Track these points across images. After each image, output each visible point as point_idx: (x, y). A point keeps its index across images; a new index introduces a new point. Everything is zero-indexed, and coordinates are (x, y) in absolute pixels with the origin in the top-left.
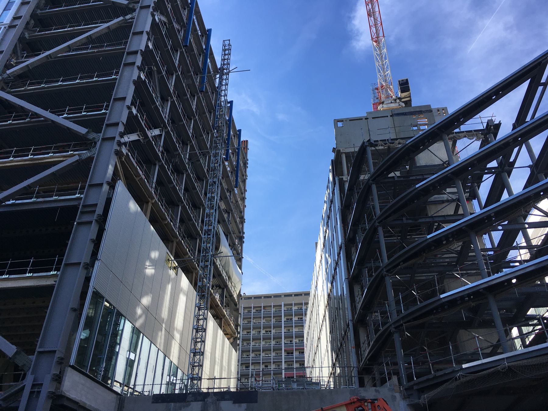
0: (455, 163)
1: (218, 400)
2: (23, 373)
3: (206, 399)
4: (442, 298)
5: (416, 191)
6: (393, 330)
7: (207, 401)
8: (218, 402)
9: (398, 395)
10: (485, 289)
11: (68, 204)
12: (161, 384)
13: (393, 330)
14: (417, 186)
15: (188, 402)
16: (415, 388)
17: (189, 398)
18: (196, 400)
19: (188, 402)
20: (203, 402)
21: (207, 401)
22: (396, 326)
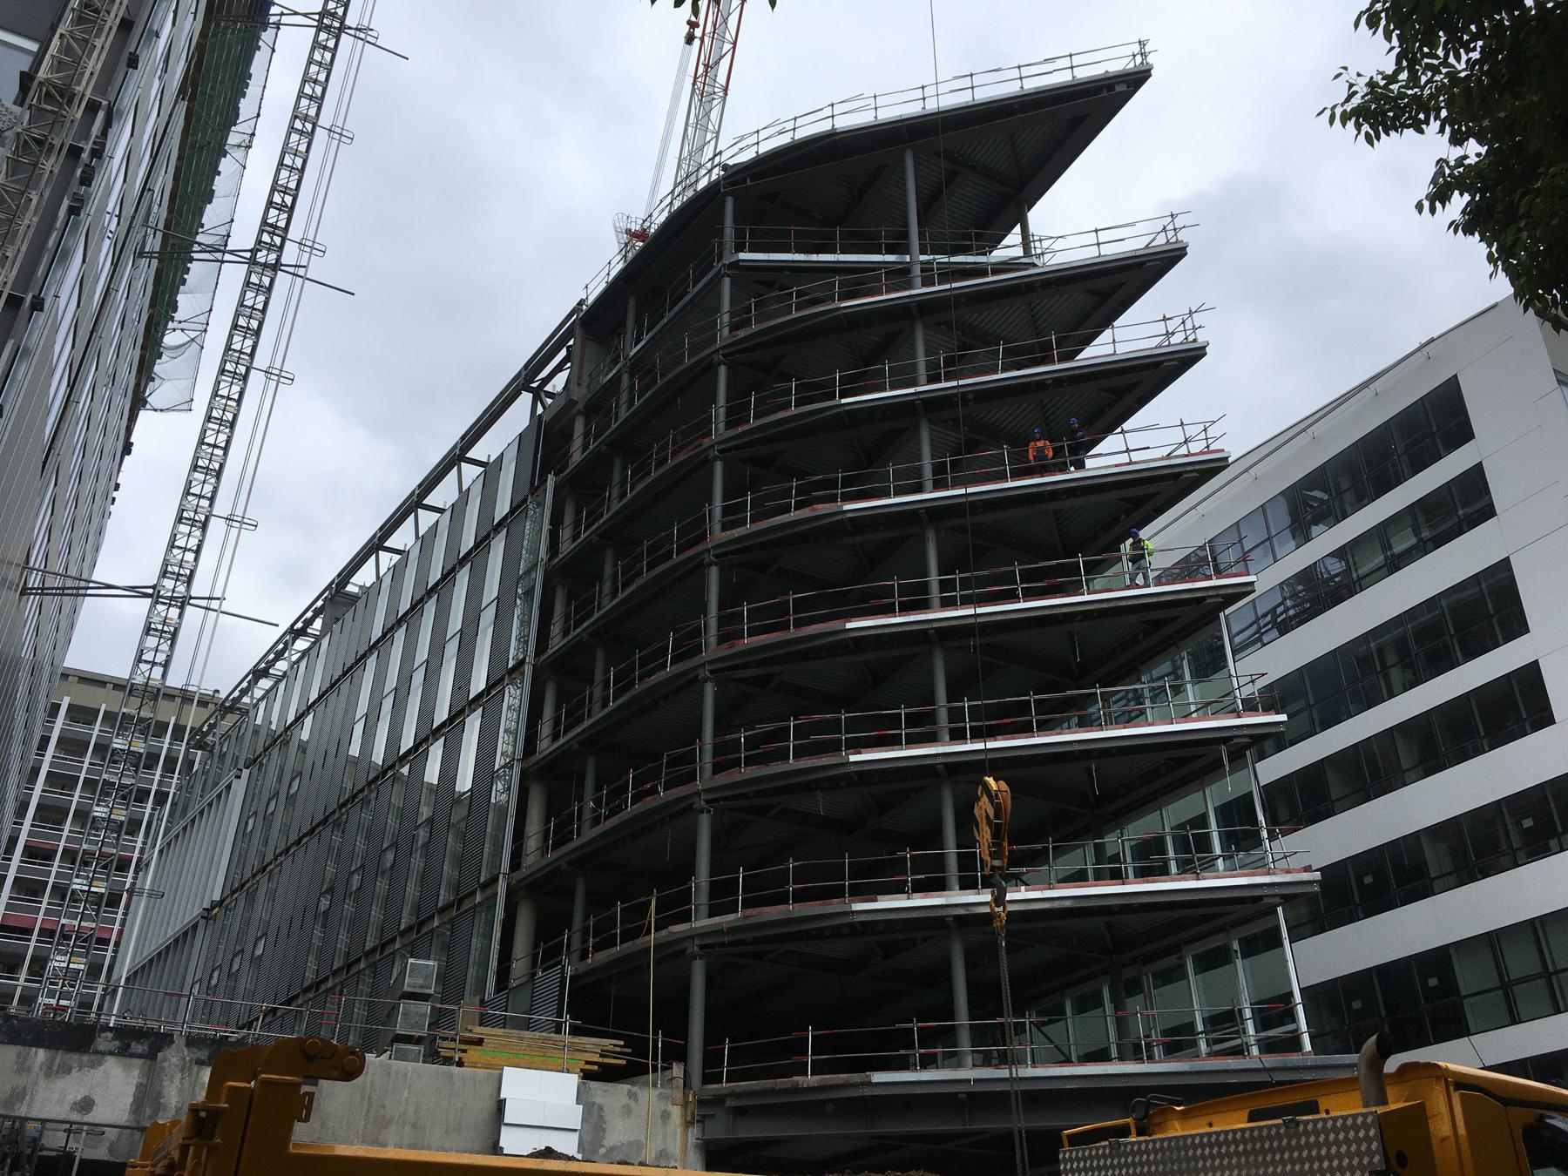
0: (1283, 503)
1: (196, 1063)
2: (1461, 513)
3: (160, 1054)
4: (853, 912)
5: (840, 637)
6: (704, 673)
7: (165, 1060)
8: (196, 1068)
9: (676, 1112)
10: (957, 918)
11: (1010, 755)
12: (1128, 451)
13: (704, 673)
14: (849, 625)
15: (97, 1052)
16: (730, 1103)
17: (104, 1042)
18: (123, 1052)
19: (97, 1052)
20: (149, 1062)
21: (165, 1060)
22: (709, 797)
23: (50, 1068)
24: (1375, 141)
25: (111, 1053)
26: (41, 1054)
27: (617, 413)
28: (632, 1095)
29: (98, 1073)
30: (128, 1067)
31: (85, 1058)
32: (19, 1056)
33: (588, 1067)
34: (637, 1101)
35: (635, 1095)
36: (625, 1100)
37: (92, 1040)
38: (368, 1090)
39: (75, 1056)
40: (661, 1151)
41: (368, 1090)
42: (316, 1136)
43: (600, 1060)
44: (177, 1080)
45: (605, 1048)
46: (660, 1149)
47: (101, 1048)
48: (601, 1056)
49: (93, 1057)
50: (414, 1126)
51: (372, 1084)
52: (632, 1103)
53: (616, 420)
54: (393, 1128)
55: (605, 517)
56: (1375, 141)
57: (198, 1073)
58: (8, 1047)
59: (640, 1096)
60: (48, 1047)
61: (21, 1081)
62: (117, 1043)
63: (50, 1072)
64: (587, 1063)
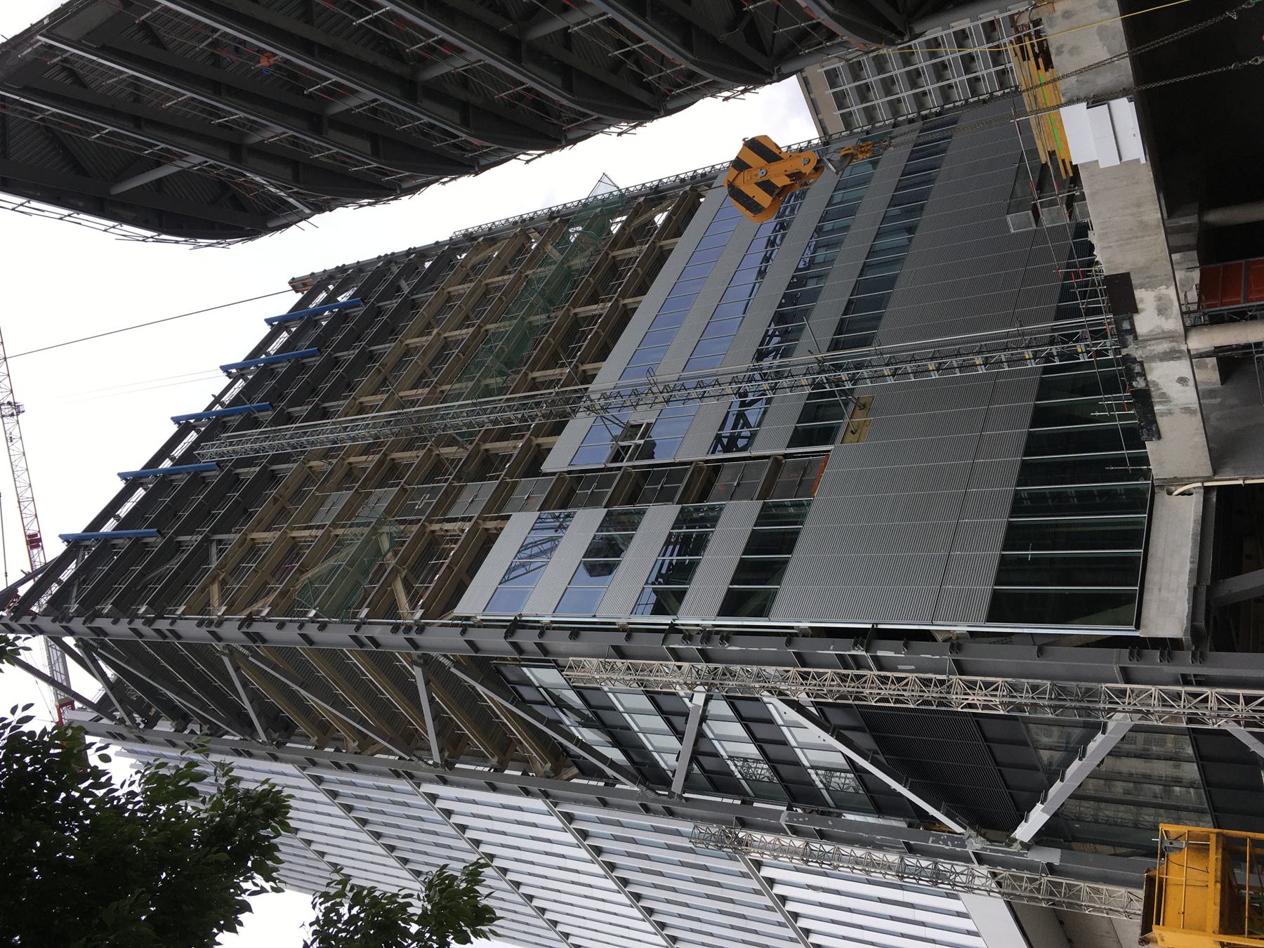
8: (1140, 338)
15: (1147, 385)
19: (1147, 385)
21: (1142, 357)
23: (1165, 402)
24: (113, 787)
25: (1146, 379)
26: (1157, 408)
27: (199, 164)
28: (1059, 52)
29: (1161, 382)
30: (1151, 369)
31: (1153, 389)
32: (1162, 416)
33: (1042, 66)
34: (1062, 46)
35: (1058, 48)
36: (1066, 56)
37: (1140, 390)
38: (1122, 242)
39: (1153, 394)
40: (1101, 8)
41: (1119, 243)
42: (1164, 262)
43: (1032, 59)
44: (1153, 348)
45: (1021, 58)
46: (1098, 10)
47: (1144, 385)
48: (1029, 59)
49: (1151, 386)
50: (1138, 205)
51: (1117, 241)
52: (1066, 49)
53: (206, 162)
54: (1145, 218)
55: (335, 78)
56: (113, 787)
57: (1142, 336)
58: (1158, 422)
59: (1058, 44)
60: (1153, 407)
61: (1177, 411)
62: (1138, 379)
63: (1165, 398)
64: (1038, 68)
